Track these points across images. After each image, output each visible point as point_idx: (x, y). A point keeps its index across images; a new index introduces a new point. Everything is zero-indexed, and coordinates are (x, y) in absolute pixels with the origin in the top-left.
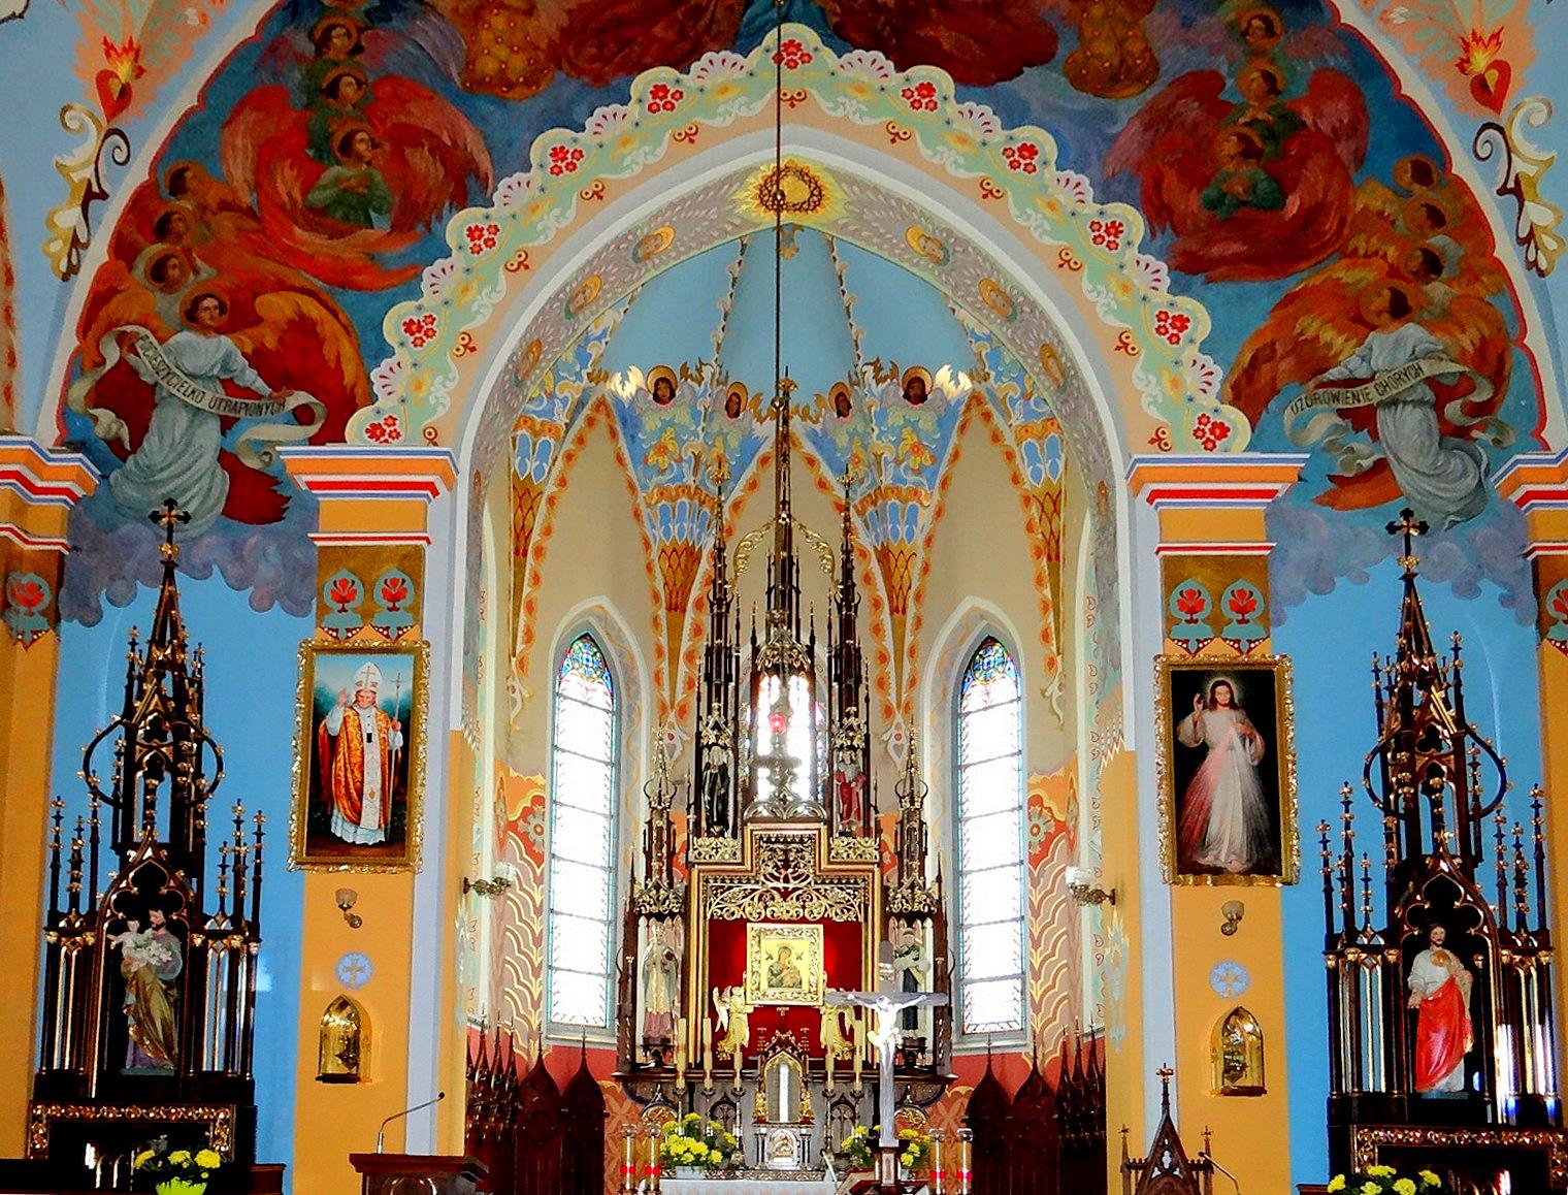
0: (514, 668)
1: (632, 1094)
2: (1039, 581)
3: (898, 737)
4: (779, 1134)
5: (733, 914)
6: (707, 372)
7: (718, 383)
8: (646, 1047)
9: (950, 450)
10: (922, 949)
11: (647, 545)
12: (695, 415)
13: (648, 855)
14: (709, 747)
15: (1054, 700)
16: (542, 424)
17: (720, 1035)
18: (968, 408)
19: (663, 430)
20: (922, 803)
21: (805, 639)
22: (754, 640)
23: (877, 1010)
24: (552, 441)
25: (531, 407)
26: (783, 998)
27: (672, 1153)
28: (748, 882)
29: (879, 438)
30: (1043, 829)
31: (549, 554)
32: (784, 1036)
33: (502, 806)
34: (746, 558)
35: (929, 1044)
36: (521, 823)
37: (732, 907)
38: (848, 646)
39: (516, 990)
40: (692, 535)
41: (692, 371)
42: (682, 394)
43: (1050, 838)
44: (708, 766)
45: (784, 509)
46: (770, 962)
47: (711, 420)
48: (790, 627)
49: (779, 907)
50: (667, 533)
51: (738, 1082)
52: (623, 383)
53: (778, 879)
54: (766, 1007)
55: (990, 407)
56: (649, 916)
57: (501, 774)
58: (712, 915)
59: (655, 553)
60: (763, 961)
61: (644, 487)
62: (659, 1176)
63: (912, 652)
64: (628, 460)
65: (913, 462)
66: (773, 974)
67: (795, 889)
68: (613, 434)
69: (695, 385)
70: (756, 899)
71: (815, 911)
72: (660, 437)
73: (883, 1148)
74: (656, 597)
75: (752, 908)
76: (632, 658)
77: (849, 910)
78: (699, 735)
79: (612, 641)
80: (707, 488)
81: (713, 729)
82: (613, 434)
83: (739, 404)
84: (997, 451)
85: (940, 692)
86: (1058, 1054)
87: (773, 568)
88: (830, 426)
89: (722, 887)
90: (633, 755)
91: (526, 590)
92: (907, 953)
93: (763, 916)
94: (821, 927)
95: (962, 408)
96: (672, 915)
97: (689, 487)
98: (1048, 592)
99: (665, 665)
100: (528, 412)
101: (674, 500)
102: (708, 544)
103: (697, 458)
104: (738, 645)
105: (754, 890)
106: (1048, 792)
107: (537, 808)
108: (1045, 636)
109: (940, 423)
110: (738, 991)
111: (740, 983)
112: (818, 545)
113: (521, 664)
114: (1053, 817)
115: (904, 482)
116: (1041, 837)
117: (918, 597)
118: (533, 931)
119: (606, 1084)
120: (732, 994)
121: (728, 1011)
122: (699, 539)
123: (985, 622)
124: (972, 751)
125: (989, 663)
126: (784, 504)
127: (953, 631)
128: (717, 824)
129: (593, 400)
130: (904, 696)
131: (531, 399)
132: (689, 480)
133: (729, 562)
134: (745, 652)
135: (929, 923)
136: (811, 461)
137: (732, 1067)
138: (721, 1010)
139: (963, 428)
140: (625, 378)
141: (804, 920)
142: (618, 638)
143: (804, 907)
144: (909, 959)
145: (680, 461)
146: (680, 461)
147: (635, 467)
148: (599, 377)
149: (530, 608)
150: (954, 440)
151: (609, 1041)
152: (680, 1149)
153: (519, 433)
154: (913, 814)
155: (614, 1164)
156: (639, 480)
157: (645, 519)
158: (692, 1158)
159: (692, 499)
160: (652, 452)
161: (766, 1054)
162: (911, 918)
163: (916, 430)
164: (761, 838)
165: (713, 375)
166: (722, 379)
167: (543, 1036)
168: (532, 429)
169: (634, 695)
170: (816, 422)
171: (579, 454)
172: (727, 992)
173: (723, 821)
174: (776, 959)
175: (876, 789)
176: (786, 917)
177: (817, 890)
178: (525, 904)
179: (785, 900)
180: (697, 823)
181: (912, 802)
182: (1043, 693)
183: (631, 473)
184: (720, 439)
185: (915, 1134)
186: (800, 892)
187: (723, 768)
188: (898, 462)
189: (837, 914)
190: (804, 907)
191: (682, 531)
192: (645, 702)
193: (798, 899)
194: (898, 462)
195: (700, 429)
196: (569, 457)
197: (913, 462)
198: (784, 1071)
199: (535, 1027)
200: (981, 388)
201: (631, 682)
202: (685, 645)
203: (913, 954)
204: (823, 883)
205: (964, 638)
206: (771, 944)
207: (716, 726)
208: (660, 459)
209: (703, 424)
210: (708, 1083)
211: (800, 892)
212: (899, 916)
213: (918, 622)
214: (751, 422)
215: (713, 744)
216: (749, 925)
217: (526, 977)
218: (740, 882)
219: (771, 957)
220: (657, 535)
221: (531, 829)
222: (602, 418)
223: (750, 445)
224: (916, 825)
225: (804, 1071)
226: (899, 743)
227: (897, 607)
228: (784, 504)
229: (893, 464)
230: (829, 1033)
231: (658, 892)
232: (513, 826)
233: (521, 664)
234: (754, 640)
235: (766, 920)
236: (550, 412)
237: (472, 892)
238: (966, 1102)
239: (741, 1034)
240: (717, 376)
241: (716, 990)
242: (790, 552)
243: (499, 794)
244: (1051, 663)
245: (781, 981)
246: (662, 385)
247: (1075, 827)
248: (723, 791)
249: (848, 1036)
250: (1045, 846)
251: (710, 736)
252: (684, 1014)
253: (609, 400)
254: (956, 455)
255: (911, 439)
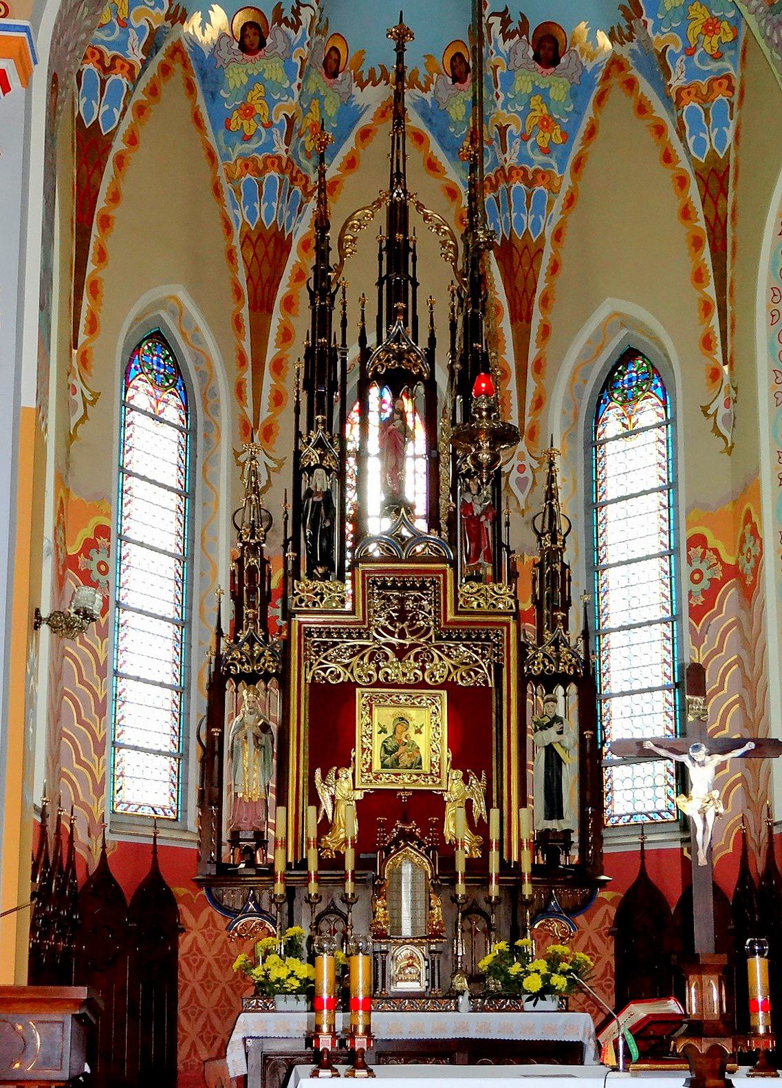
0: (75, 364)
1: (217, 902)
2: (699, 277)
3: (521, 469)
4: (404, 952)
5: (338, 676)
6: (306, 15)
7: (318, 32)
8: (235, 839)
9: (584, 127)
10: (565, 721)
11: (228, 229)
12: (288, 68)
13: (237, 598)
14: (310, 470)
15: (719, 418)
16: (114, 58)
17: (325, 827)
18: (607, 75)
19: (249, 87)
20: (564, 541)
21: (423, 345)
22: (363, 340)
23: (688, 764)
24: (125, 81)
25: (98, 35)
26: (405, 782)
27: (273, 978)
28: (360, 637)
29: (504, 106)
30: (707, 575)
31: (116, 225)
32: (408, 828)
33: (61, 532)
34: (353, 241)
35: (575, 838)
36: (81, 558)
37: (336, 669)
38: (475, 351)
39: (76, 772)
40: (281, 217)
41: (287, 14)
42: (275, 46)
43: (716, 585)
44: (310, 493)
45: (399, 182)
46: (384, 736)
47: (307, 76)
48: (406, 325)
49: (393, 669)
50: (252, 214)
51: (349, 886)
52: (203, 25)
53: (392, 634)
54: (378, 792)
55: (634, 72)
56: (238, 678)
57: (62, 494)
58: (313, 678)
59: (236, 242)
60: (376, 735)
61: (227, 156)
62: (368, 1011)
63: (538, 366)
64: (207, 123)
65: (542, 139)
66: (386, 751)
67: (413, 646)
68: (190, 87)
69: (289, 31)
70: (366, 659)
71: (437, 674)
72: (245, 97)
73: (703, 965)
74: (238, 292)
75: (361, 670)
76: (211, 366)
77: (476, 673)
78: (297, 454)
79: (185, 339)
80: (299, 163)
81: (315, 447)
82: (190, 87)
83: (338, 61)
84: (642, 127)
85: (571, 413)
86: (730, 850)
87: (384, 253)
88: (443, 95)
89: (326, 642)
90: (210, 485)
91: (91, 267)
92: (550, 725)
93: (375, 679)
94: (444, 693)
95: (600, 75)
96: (267, 677)
97: (279, 158)
98: (711, 291)
99: (248, 375)
100: (95, 41)
101: (260, 173)
102: (302, 228)
103: (290, 122)
104: (344, 344)
105: (363, 647)
106: (711, 529)
107: (101, 541)
108: (707, 343)
109: (573, 95)
110: (346, 773)
111: (347, 762)
112: (438, 228)
113: (84, 360)
114: (719, 559)
115: (531, 162)
116: (705, 584)
117: (545, 302)
118: (95, 695)
119: (179, 891)
120: (337, 777)
121: (333, 797)
122: (289, 225)
123: (624, 332)
124: (612, 487)
125: (630, 380)
126: (398, 177)
127: (589, 342)
128: (321, 565)
129: (167, 45)
130: (528, 420)
131: (102, 26)
132: (280, 149)
133: (333, 244)
134: (353, 353)
135: (573, 688)
136: (419, 138)
137: (342, 867)
138: (325, 796)
139: (600, 99)
140: (206, 19)
141: (423, 685)
142: (195, 338)
143: (423, 669)
144: (552, 731)
145: (269, 125)
146: (269, 125)
147: (216, 134)
148: (178, 16)
149: (95, 292)
150: (589, 112)
151: (187, 836)
152: (282, 973)
153: (86, 67)
154: (553, 555)
155: (187, 994)
156: (220, 149)
157: (226, 196)
158: (297, 984)
159: (282, 172)
160: (235, 114)
161: (388, 850)
162: (549, 681)
163: (546, 100)
164: (374, 582)
165: (313, 18)
166: (322, 26)
167: (107, 829)
168: (100, 62)
169: (212, 409)
170: (425, 90)
171: (152, 107)
172: (332, 774)
173: (327, 560)
174: (390, 733)
175: (508, 524)
176: (403, 680)
177: (439, 648)
178: (86, 661)
179: (400, 660)
180: (297, 563)
181: (554, 540)
182: (705, 409)
183: (211, 139)
184: (316, 102)
185: (566, 950)
186: (419, 649)
187: (327, 495)
188: (525, 138)
189: (462, 678)
190: (423, 669)
191: (268, 212)
192: (320, 626)
193: (416, 659)
194: (525, 138)
195: (295, 85)
196: (141, 110)
197: (542, 139)
198: (407, 870)
199: (97, 819)
200: (624, 51)
201: (210, 394)
202: (272, 352)
203: (556, 727)
204: (449, 638)
205: (601, 348)
206: (384, 716)
207: (320, 444)
208: (245, 123)
209: (299, 80)
210: (313, 888)
211: (419, 649)
212: (538, 680)
213: (546, 331)
214: (350, 87)
215: (317, 466)
216: (358, 691)
217: (87, 754)
218: (349, 637)
219: (383, 731)
220: (239, 215)
221: (93, 566)
222: (177, 67)
223: (349, 114)
224: (559, 568)
225: (433, 870)
226: (522, 476)
227: (521, 313)
228: (398, 177)
229: (519, 140)
230: (454, 826)
231: (252, 647)
232: (71, 562)
233: (84, 360)
234: (363, 340)
235: (378, 684)
236: (122, 45)
237: (45, 629)
238: (613, 912)
239: (348, 826)
240: (317, 21)
241: (318, 772)
242: (406, 234)
243: (59, 518)
244: (715, 374)
245: (397, 760)
246: (249, 31)
247: (756, 571)
248: (328, 524)
249: (479, 828)
250: (710, 595)
251: (313, 456)
252: (282, 800)
253: (186, 46)
254: (591, 133)
255: (539, 110)
